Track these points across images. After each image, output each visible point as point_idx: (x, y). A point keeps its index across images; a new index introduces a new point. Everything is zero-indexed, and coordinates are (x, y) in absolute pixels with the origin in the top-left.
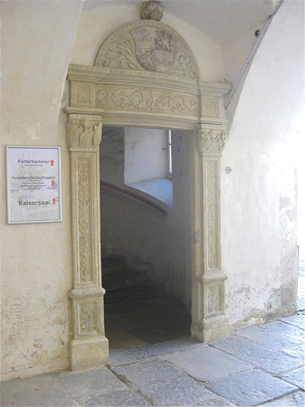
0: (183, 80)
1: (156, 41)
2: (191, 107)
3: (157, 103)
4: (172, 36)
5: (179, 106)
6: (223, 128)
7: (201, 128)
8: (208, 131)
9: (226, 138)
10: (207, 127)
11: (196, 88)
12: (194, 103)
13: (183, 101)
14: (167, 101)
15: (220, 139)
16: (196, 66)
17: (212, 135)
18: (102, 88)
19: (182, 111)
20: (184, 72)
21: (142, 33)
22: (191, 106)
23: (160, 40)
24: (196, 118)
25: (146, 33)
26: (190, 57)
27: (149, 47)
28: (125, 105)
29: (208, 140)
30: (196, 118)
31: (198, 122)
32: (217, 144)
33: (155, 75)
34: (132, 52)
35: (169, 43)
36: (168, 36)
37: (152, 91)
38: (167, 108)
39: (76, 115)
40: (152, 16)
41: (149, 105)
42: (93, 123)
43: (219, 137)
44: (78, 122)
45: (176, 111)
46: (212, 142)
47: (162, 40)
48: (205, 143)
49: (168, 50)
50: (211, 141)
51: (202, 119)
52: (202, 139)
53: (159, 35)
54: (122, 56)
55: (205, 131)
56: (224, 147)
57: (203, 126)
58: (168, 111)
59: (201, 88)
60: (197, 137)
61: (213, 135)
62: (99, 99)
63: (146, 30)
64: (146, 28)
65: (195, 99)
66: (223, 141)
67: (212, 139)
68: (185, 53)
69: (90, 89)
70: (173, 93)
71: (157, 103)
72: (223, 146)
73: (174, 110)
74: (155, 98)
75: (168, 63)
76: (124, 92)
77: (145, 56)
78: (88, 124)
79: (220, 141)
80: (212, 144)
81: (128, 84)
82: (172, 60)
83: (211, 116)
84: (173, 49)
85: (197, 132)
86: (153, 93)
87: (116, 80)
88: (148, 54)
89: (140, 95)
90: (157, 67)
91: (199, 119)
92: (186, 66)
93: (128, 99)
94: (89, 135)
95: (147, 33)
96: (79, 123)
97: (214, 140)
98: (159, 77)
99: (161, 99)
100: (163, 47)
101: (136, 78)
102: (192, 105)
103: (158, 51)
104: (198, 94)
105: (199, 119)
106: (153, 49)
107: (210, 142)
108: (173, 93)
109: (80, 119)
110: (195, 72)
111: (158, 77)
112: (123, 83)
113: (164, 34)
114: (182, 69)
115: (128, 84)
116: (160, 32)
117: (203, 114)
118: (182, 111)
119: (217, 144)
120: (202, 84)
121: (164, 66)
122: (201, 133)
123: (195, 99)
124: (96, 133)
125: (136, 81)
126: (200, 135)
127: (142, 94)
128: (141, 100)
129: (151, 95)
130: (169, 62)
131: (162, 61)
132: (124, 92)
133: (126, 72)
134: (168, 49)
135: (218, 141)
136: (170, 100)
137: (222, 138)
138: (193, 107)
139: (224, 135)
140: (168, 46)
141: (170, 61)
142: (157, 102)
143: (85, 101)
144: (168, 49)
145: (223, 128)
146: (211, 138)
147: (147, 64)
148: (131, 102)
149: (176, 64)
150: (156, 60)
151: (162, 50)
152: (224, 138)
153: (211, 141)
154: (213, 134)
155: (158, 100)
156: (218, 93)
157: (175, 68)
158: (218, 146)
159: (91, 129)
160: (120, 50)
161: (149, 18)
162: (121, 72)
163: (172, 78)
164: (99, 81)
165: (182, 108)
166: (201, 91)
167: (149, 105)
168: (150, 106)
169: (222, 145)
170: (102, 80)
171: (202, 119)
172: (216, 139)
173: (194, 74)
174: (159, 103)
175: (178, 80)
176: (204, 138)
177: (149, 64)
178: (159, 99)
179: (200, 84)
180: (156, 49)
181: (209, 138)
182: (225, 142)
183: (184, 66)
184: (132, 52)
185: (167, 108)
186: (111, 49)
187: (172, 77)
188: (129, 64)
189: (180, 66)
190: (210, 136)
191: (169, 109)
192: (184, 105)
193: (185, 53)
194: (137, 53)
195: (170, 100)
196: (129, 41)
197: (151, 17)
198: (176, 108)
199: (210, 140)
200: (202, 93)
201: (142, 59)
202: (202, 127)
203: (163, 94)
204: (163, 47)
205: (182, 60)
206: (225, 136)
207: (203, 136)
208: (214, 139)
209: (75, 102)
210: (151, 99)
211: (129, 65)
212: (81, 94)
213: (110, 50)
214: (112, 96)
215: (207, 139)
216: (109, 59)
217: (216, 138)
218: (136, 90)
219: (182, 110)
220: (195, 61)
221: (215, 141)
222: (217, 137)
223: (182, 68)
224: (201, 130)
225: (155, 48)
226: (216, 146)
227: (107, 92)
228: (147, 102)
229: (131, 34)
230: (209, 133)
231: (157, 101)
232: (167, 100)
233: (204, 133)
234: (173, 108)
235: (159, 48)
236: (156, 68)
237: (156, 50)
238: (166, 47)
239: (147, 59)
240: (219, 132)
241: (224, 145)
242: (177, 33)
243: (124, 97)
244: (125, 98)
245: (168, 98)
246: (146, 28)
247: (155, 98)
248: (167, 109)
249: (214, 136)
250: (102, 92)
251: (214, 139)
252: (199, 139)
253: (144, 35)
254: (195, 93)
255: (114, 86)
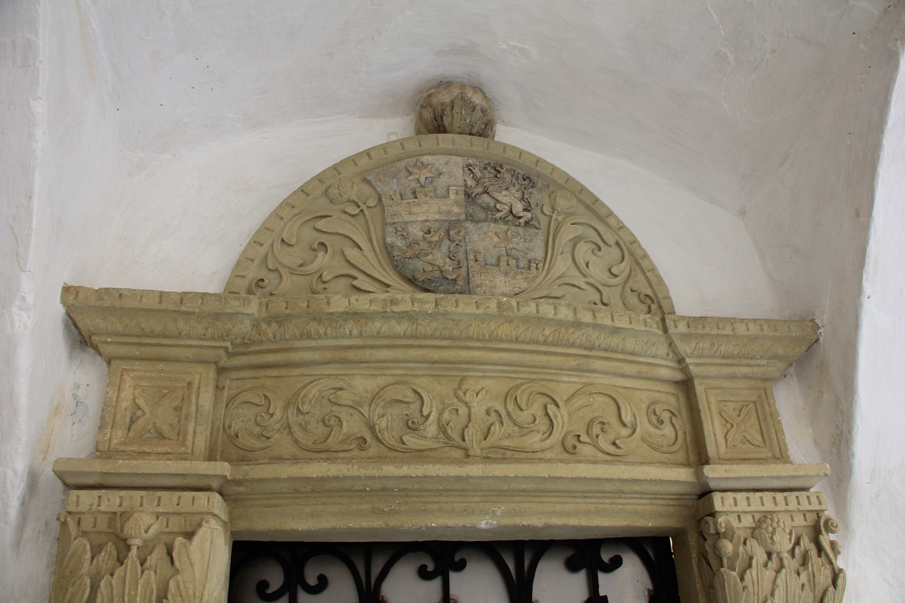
0: (595, 317)
1: (468, 195)
2: (657, 431)
3: (493, 424)
4: (535, 179)
5: (596, 429)
6: (814, 500)
7: (713, 514)
8: (748, 521)
9: (840, 543)
10: (742, 506)
11: (663, 350)
12: (666, 416)
13: (613, 408)
14: (540, 414)
15: (813, 552)
16: (649, 274)
17: (772, 538)
18: (249, 384)
19: (612, 449)
20: (601, 294)
21: (410, 173)
22: (656, 427)
23: (486, 192)
24: (683, 475)
25: (423, 176)
26: (617, 244)
27: (437, 217)
28: (343, 442)
29: (754, 562)
30: (683, 475)
31: (698, 490)
32: (804, 577)
33: (457, 302)
34: (371, 240)
35: (522, 199)
36: (517, 179)
37: (464, 378)
38: (542, 440)
39: (95, 493)
40: (447, 121)
41: (455, 435)
42: (176, 524)
43: (806, 543)
44: (103, 525)
45: (587, 450)
46: (778, 572)
47: (491, 189)
48: (742, 579)
49: (521, 221)
50: (773, 564)
51: (713, 473)
52: (725, 561)
53: (479, 174)
54: (327, 256)
55: (735, 523)
56: (843, 590)
57: (719, 502)
58: (548, 455)
59: (684, 348)
60: (703, 555)
61: (777, 538)
62: (230, 427)
63: (424, 166)
64: (426, 159)
65: (669, 398)
66: (831, 563)
67: (774, 556)
68: (596, 230)
69: (190, 384)
70: (565, 379)
71: (493, 424)
72: (834, 583)
73: (575, 447)
74: (479, 408)
75: (523, 263)
76: (340, 389)
77: (424, 245)
78: (146, 532)
79: (815, 560)
80: (779, 581)
81: (350, 355)
82: (539, 254)
83: (749, 459)
84: (543, 220)
85: (702, 536)
86: (468, 385)
87: (298, 344)
88: (436, 238)
89: (410, 396)
90: (477, 279)
91: (699, 474)
92: (608, 274)
93: (357, 416)
94: (141, 581)
95: (429, 175)
96: (106, 529)
97: (786, 562)
98: (477, 308)
99: (511, 407)
100: (499, 211)
101: (378, 324)
102: (662, 422)
103: (480, 224)
104: (679, 376)
105: (699, 474)
106: (458, 221)
107: (769, 574)
108: (565, 379)
109: (115, 509)
110: (649, 292)
111: (472, 309)
112: (328, 355)
113: (499, 172)
114: (587, 283)
115: (350, 355)
116: (485, 168)
117: (711, 451)
118: (612, 449)
119: (804, 577)
120: (682, 328)
121: (506, 274)
122: (718, 533)
123: (672, 400)
124: (177, 571)
125: (378, 335)
126: (715, 547)
127: (419, 390)
128: (417, 414)
129: (460, 393)
130: (530, 261)
131: (499, 259)
132: (340, 389)
133: (328, 303)
134: (520, 218)
135: (804, 562)
136: (551, 409)
137: (820, 549)
138: (668, 431)
139: (828, 530)
140: (518, 208)
141: (531, 255)
142: (493, 417)
143: (161, 436)
144: (520, 218)
145: (814, 500)
146: (769, 555)
147: (431, 271)
148: (372, 428)
149: (562, 264)
150: (471, 257)
151: (496, 221)
152: (833, 544)
153: (773, 564)
154: (773, 533)
155: (497, 411)
156: (764, 362)
157: (559, 282)
158: (813, 587)
159: (157, 556)
160: (324, 238)
161: (440, 129)
162: (308, 307)
163: (538, 311)
164: (230, 355)
165: (611, 437)
166: (688, 361)
167: (455, 435)
168: (460, 440)
169: (830, 581)
170: (244, 346)
171: (713, 473)
172: (793, 556)
173: (648, 301)
174: (502, 423)
175: (570, 317)
176: (736, 555)
177: (442, 271)
178: (500, 408)
179: (671, 330)
180: (470, 218)
181: (760, 556)
182: (840, 563)
183: (597, 272)
184: (371, 240)
185: (542, 440)
186: (285, 236)
187: (540, 309)
188: (355, 278)
189: (578, 274)
190: (761, 543)
191: (552, 447)
192: (625, 425)
193: (596, 230)
194: (389, 240)
195: (551, 409)
196: (360, 204)
197: (444, 126)
198: (584, 438)
199: (766, 565)
200: (691, 367)
201: (410, 258)
202: (718, 506)
203: (517, 387)
204: (499, 211)
205: (583, 251)
206: (832, 537)
207: (728, 547)
208: (786, 556)
209: (115, 441)
210: (463, 411)
211: (355, 283)
212: (147, 410)
213: (283, 240)
214: (286, 408)
215: (751, 558)
216: (277, 270)
217: (793, 549)
218: (394, 379)
219: (614, 444)
220: (645, 256)
221: (792, 564)
222: (797, 543)
223: (591, 280)
224: (715, 524)
225: (463, 217)
226: (803, 585)
227: (265, 396)
228: (444, 422)
229: (369, 183)
230: (755, 531)
231: (493, 414)
232: (536, 409)
233: (729, 534)
234: (571, 441)
235: (482, 215)
236: (471, 285)
237: (470, 226)
238: (511, 212)
239: (430, 257)
240: (799, 521)
241: (840, 582)
242: (554, 168)
243: (335, 408)
244: (344, 414)
245: (543, 400)
246: (426, 159)
247: (479, 408)
248: (537, 446)
249: (783, 543)
250: (245, 397)
251: (786, 556)
252: (714, 567)
253: (418, 180)
254: (665, 373)
255: (297, 372)
